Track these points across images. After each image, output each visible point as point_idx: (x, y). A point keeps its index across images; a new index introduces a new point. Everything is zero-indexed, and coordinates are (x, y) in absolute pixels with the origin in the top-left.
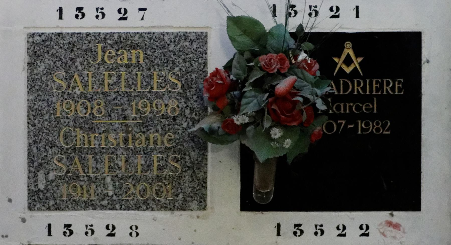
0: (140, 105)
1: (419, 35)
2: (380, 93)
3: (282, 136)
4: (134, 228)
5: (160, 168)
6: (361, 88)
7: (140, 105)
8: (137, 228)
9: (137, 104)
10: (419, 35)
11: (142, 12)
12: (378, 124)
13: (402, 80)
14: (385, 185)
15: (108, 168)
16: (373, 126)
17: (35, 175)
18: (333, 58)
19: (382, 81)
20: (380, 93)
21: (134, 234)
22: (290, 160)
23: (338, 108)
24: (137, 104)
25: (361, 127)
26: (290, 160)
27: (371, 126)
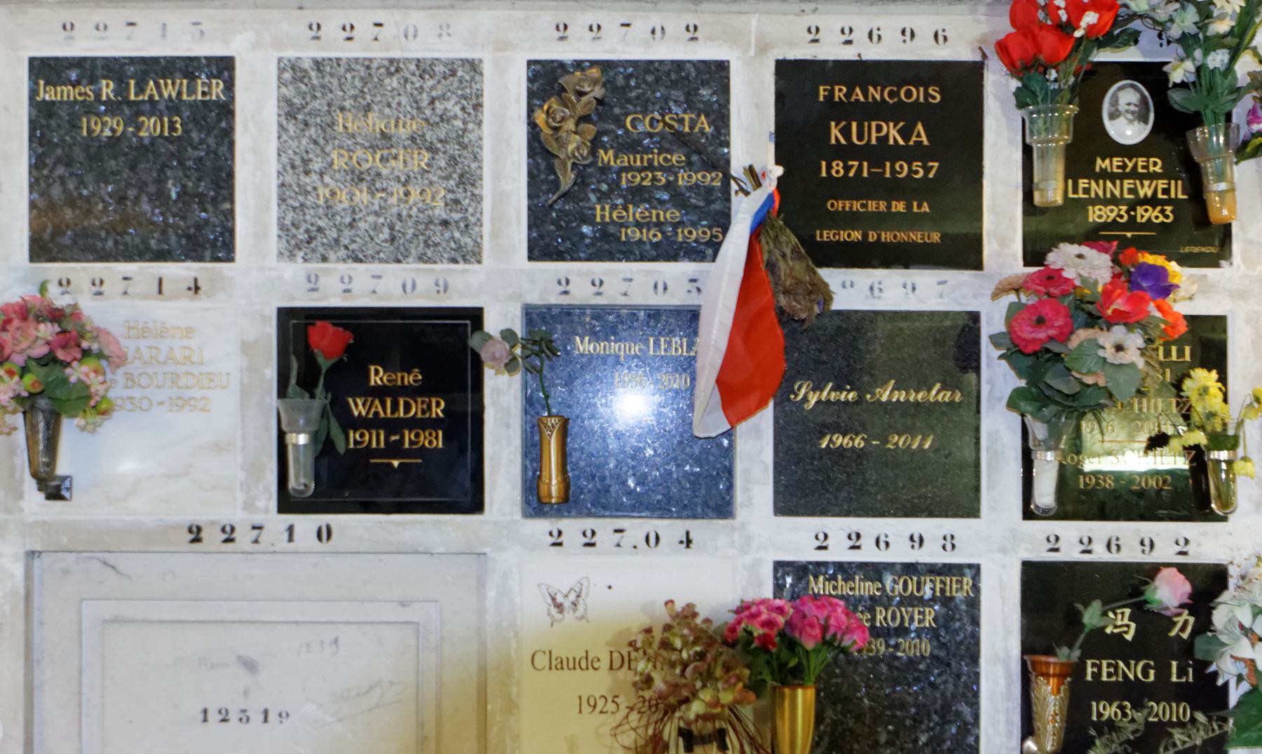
0: (686, 232)
1: (1026, 564)
2: (427, 415)
3: (349, 349)
4: (949, 538)
5: (920, 621)
6: (442, 411)
7: (686, 232)
9: (683, 232)
10: (1026, 564)
12: (430, 434)
13: (1152, 663)
14: (715, 332)
15: (273, 243)
16: (425, 438)
17: (37, 84)
18: (771, 404)
19: (430, 402)
20: (1184, 680)
21: (949, 546)
22: (1149, 606)
24: (683, 232)
25: (410, 439)
26: (1149, 606)
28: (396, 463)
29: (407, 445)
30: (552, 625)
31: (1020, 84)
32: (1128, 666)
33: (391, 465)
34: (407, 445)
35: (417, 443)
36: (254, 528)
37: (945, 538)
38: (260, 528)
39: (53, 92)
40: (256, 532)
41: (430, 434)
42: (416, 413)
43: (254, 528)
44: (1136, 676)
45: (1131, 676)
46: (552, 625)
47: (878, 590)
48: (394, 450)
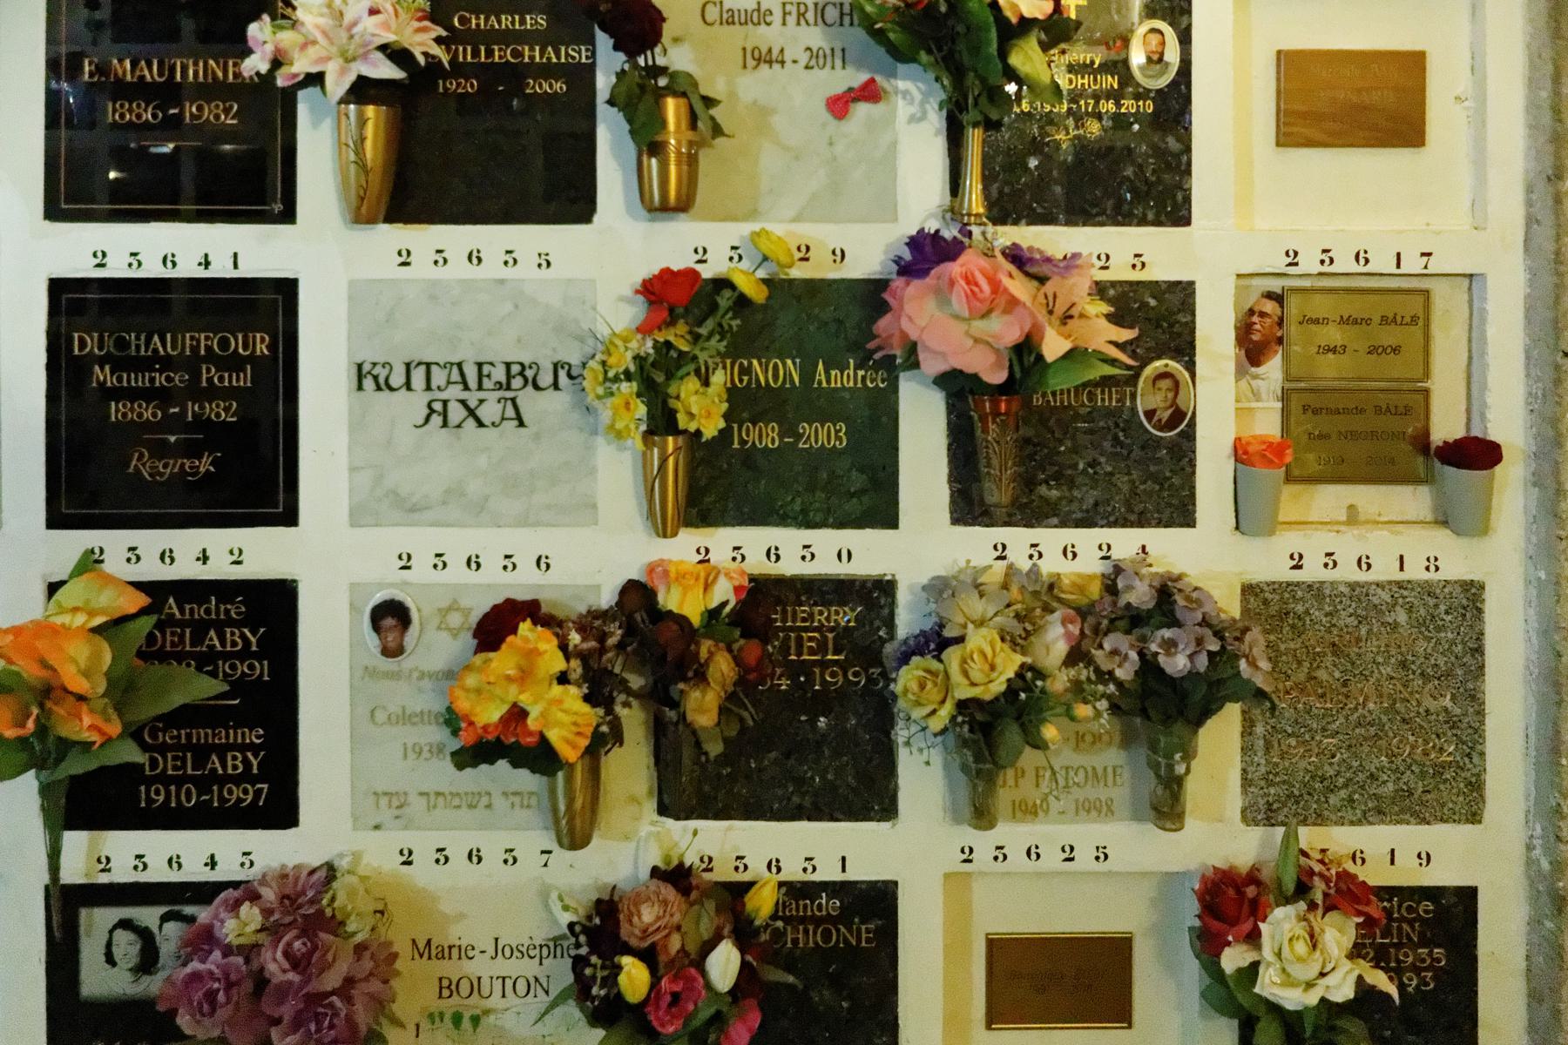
4: (1432, 560)
8: (1436, 559)
11: (546, 856)
12: (122, 106)
16: (211, 409)
23: (120, 379)
27: (208, 410)
28: (172, 439)
29: (188, 120)
30: (421, 794)
31: (682, 321)
32: (846, 941)
33: (166, 441)
34: (188, 120)
35: (199, 117)
36: (1423, 254)
37: (1428, 559)
38: (1429, 254)
39: (794, 906)
40: (1425, 258)
41: (122, 106)
42: (92, 348)
43: (1423, 254)
44: (838, 931)
45: (843, 929)
46: (421, 794)
47: (258, 737)
48: (171, 126)
